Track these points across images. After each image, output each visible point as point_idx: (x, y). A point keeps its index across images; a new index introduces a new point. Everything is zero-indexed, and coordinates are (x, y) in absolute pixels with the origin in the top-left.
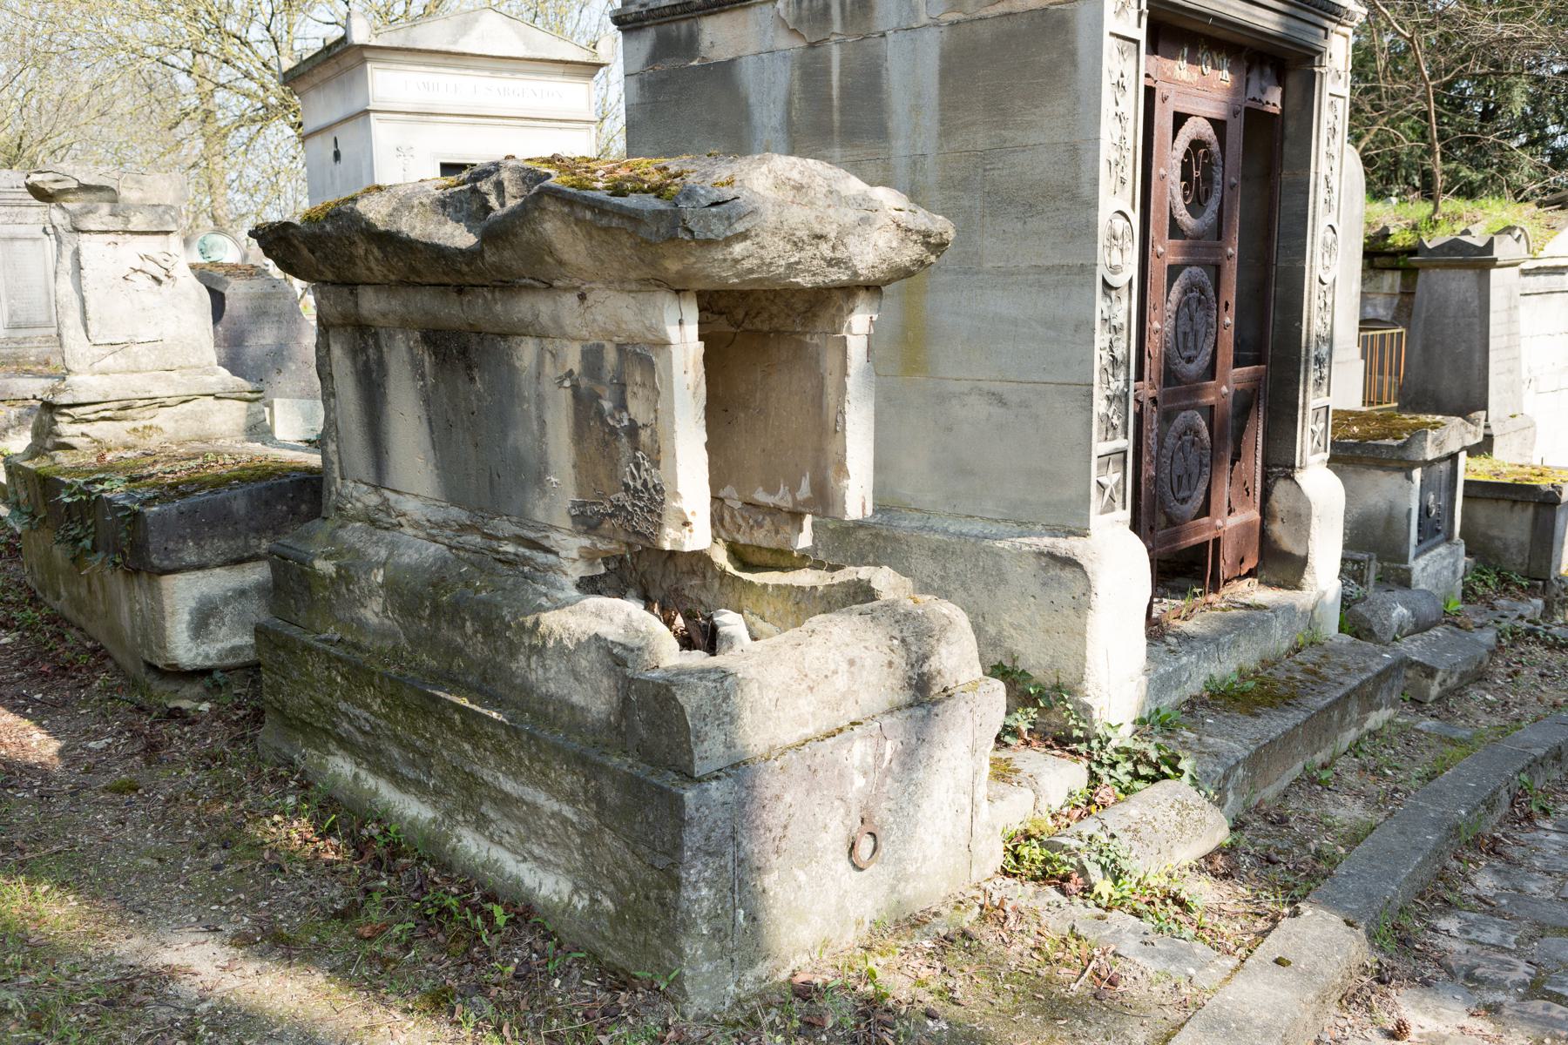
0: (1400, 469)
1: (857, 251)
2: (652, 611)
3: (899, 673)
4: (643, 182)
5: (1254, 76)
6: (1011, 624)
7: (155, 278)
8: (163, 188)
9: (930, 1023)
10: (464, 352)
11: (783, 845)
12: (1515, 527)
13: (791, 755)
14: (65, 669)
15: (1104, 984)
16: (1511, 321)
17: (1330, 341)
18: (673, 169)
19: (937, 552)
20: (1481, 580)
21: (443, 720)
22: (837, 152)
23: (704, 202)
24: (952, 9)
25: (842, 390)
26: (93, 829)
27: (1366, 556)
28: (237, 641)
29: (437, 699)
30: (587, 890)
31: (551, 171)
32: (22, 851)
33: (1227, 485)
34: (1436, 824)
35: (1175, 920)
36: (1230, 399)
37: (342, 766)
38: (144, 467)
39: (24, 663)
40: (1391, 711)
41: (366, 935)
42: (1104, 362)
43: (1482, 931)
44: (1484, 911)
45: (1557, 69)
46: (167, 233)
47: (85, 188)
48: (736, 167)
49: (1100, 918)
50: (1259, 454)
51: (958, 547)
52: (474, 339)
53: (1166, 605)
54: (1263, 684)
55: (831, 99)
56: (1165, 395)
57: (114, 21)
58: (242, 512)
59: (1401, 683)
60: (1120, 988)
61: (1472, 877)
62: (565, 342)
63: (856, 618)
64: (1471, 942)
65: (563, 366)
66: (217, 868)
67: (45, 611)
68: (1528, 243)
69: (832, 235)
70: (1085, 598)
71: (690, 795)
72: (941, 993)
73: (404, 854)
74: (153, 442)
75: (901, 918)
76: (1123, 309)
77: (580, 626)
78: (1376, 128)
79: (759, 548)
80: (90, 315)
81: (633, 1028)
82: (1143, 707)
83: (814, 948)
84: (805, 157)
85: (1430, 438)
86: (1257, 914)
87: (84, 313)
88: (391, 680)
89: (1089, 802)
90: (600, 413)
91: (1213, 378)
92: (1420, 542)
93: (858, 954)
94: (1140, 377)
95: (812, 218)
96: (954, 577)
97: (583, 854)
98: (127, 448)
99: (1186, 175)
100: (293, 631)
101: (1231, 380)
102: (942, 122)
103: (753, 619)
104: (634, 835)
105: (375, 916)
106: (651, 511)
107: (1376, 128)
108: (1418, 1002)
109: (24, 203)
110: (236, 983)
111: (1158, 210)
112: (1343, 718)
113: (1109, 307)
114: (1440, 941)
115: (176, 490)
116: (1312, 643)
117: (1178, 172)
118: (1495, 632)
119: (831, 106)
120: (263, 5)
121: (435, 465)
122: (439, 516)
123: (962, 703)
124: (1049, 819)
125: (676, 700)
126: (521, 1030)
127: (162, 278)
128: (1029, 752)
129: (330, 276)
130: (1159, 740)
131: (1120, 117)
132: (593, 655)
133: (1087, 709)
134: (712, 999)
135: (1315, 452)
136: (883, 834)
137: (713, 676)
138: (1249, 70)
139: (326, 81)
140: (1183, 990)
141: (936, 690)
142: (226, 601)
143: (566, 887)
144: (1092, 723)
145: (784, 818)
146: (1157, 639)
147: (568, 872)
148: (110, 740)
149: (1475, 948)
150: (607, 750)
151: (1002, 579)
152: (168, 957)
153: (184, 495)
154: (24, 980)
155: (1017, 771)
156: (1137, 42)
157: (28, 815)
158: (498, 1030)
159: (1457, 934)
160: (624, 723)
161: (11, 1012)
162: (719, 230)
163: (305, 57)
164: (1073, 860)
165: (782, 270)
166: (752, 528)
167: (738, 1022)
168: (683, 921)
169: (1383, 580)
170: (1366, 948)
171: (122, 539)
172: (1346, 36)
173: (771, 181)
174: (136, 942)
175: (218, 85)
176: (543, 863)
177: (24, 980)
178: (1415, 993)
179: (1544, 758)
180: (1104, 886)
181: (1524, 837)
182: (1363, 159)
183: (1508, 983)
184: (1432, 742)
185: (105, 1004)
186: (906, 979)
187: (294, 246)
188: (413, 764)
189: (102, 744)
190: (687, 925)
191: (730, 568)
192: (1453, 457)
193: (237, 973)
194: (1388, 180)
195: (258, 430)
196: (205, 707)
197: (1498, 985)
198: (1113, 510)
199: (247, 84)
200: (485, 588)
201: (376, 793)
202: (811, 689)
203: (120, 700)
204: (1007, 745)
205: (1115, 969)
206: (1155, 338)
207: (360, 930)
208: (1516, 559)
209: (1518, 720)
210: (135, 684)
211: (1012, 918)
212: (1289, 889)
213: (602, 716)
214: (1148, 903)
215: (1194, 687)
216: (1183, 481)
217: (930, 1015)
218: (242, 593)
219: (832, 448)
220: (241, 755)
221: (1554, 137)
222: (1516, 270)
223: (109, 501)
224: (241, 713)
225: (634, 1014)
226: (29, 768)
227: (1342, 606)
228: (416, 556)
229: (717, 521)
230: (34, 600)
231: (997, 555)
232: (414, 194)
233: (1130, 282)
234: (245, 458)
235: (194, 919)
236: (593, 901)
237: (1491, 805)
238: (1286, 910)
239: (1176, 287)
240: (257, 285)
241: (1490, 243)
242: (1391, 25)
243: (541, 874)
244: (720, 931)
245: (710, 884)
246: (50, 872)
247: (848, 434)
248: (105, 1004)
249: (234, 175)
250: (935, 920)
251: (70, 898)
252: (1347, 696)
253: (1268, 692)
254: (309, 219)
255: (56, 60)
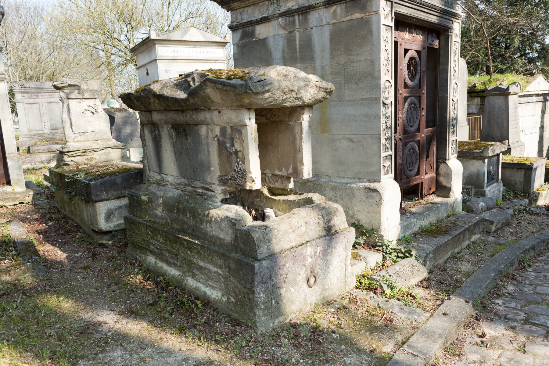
0: (481, 159)
1: (304, 95)
2: (245, 209)
3: (321, 226)
4: (237, 76)
5: (430, 37)
6: (357, 210)
7: (92, 112)
8: (95, 85)
9: (334, 335)
10: (184, 130)
11: (286, 280)
12: (518, 177)
13: (288, 252)
14: (68, 232)
15: (388, 322)
16: (516, 112)
17: (456, 119)
18: (246, 71)
19: (334, 189)
20: (508, 194)
21: (181, 244)
22: (299, 65)
23: (255, 81)
24: (333, 19)
25: (301, 138)
26: (76, 280)
27: (471, 187)
28: (119, 222)
29: (179, 238)
30: (226, 295)
31: (209, 74)
32: (55, 287)
33: (425, 165)
34: (494, 270)
35: (411, 302)
36: (425, 138)
37: (151, 259)
38: (90, 170)
39: (56, 231)
40: (479, 235)
41: (159, 311)
42: (384, 127)
43: (509, 303)
44: (510, 297)
45: (529, 32)
46: (95, 98)
47: (70, 86)
48: (265, 70)
49: (387, 301)
50: (435, 155)
51: (340, 187)
52: (187, 126)
53: (406, 204)
54: (438, 227)
55: (296, 49)
56: (404, 138)
57: (80, 35)
58: (120, 182)
59: (482, 226)
60: (393, 323)
61: (506, 287)
62: (215, 126)
63: (307, 209)
64: (506, 307)
65: (215, 134)
66: (114, 291)
67: (62, 215)
68: (521, 87)
69: (296, 90)
70: (380, 202)
71: (256, 265)
72: (337, 325)
73: (171, 286)
74: (93, 162)
75: (324, 302)
76: (390, 111)
77: (222, 214)
78: (471, 53)
79: (278, 189)
80: (73, 124)
81: (241, 338)
82: (400, 235)
83: (297, 312)
84: (287, 66)
85: (490, 149)
86: (437, 299)
87: (71, 124)
88: (165, 232)
89: (383, 265)
90: (226, 147)
91: (419, 132)
92: (488, 182)
93: (311, 314)
94: (396, 132)
95: (289, 85)
96: (339, 196)
97: (225, 284)
98: (85, 164)
99: (409, 67)
100: (136, 218)
101: (424, 133)
102: (331, 54)
103: (276, 210)
104: (240, 278)
105: (162, 305)
106: (242, 178)
107: (471, 53)
108: (489, 326)
109: (54, 91)
110: (120, 326)
111: (400, 80)
112: (464, 237)
113: (385, 110)
114: (496, 307)
115: (100, 176)
116: (453, 214)
117: (406, 67)
118: (513, 210)
119: (297, 51)
120: (125, 29)
121: (177, 166)
122: (178, 182)
123: (342, 235)
124: (370, 271)
125: (251, 236)
126: (207, 339)
127: (94, 112)
128: (364, 250)
129: (143, 109)
130: (405, 245)
131: (386, 51)
132: (226, 223)
133: (382, 236)
134: (265, 328)
135: (453, 154)
136: (318, 276)
137: (263, 228)
138: (428, 35)
139: (143, 51)
140: (413, 323)
141: (333, 231)
142: (116, 210)
143: (220, 295)
144: (383, 241)
145: (286, 272)
146: (404, 214)
147: (220, 290)
148: (82, 253)
149: (507, 309)
150: (231, 252)
151: (354, 196)
152: (99, 319)
153: (102, 178)
154: (56, 326)
155: (360, 256)
156: (391, 27)
157: (57, 277)
158: (200, 339)
159: (501, 305)
160: (236, 243)
161: (52, 336)
162: (260, 89)
163: (137, 44)
164: (378, 283)
165: (281, 101)
166: (275, 182)
167: (274, 335)
168: (255, 304)
169: (477, 195)
170: (472, 309)
171: (84, 192)
172: (459, 23)
173: (276, 74)
174: (90, 314)
175: (112, 54)
176: (213, 287)
177: (56, 326)
178: (488, 323)
179: (529, 249)
180: (388, 291)
181: (523, 274)
182: (467, 62)
183: (518, 320)
184: (493, 244)
185: (80, 333)
186: (326, 321)
187: (132, 100)
188: (173, 258)
189: (79, 254)
190: (257, 305)
191: (269, 195)
192: (498, 155)
193: (120, 323)
194: (476, 69)
195: (125, 158)
196: (110, 242)
197: (515, 320)
198: (388, 174)
199: (120, 53)
200: (193, 203)
201: (162, 267)
202: (294, 231)
203: (85, 241)
204: (357, 248)
205: (392, 317)
206: (400, 120)
207: (157, 309)
208: (519, 187)
209: (521, 237)
210: (89, 236)
211: (359, 302)
212: (447, 291)
213: (229, 241)
214: (402, 296)
215: (416, 229)
216: (410, 165)
217: (334, 332)
218: (120, 207)
219: (299, 156)
220: (121, 257)
221: (529, 53)
222: (517, 96)
223: (80, 180)
224: (121, 244)
225: (241, 333)
226: (57, 262)
227: (463, 202)
228: (172, 194)
229: (263, 180)
230: (59, 212)
231: (352, 189)
232: (168, 82)
233: (392, 102)
234: (121, 166)
235: (107, 307)
236: (228, 299)
237: (512, 264)
238: (446, 298)
239: (407, 104)
240: (124, 114)
241: (508, 88)
242: (475, 20)
243: (212, 291)
244: (267, 307)
245: (264, 292)
246: (64, 294)
247: (303, 152)
248: (80, 333)
249: (117, 81)
250: (335, 303)
251: (70, 301)
252: (465, 231)
253: (439, 230)
254: (136, 92)
255: (63, 49)
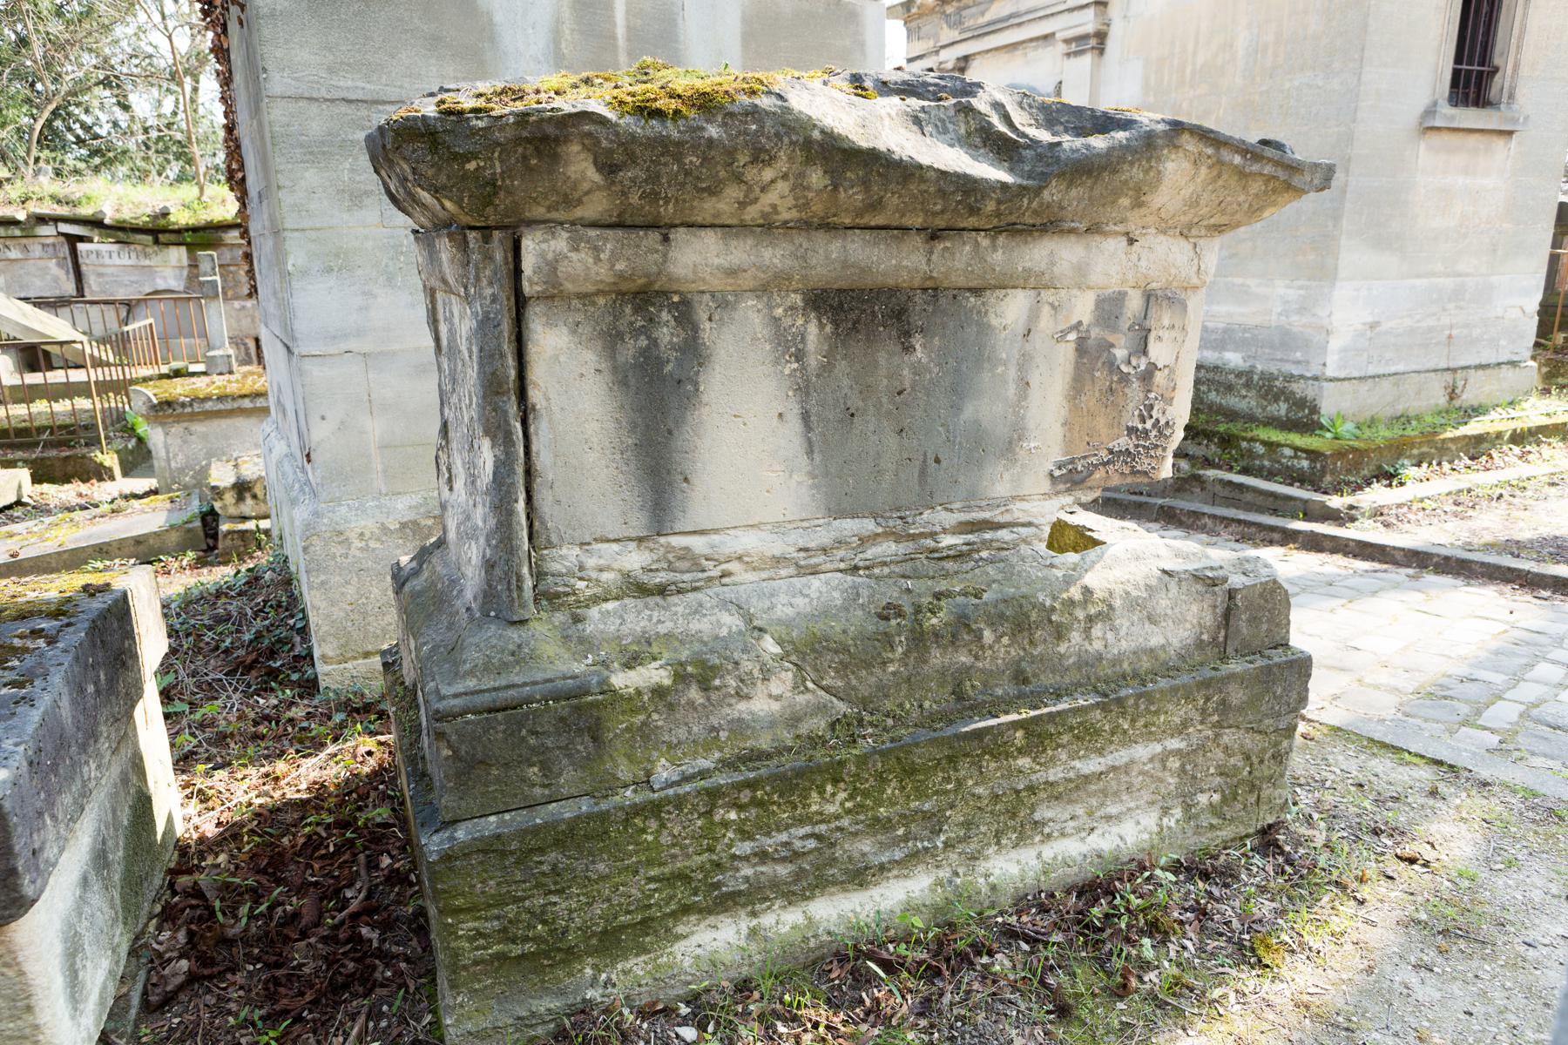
55: (613, 37)
62: (1075, 292)
119: (615, 47)
143: (1150, 820)
243: (1115, 830)
